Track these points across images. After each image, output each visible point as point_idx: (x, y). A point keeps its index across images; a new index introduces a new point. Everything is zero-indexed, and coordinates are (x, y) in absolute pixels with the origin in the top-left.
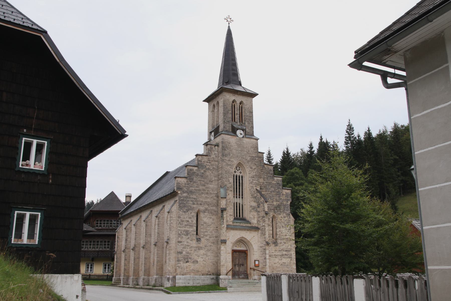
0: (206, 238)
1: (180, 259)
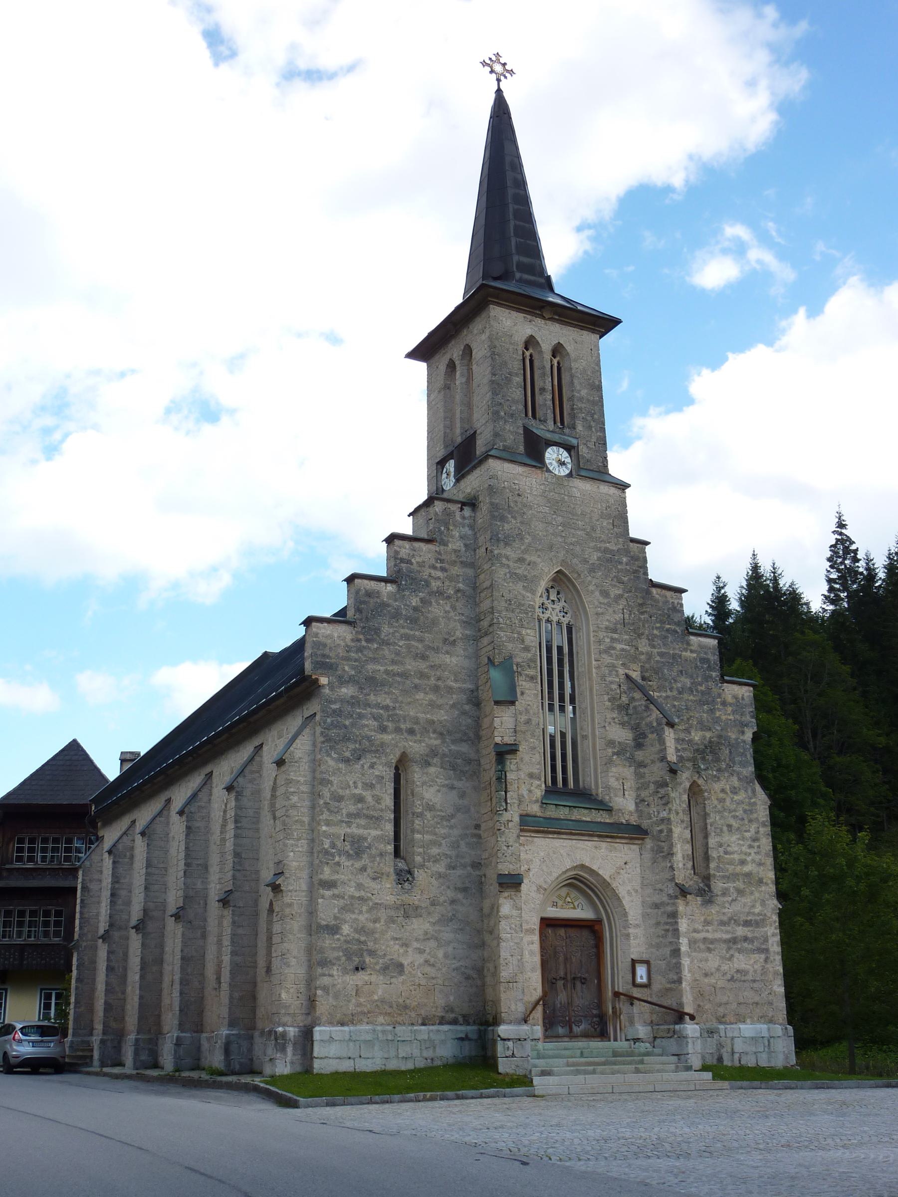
0: (435, 869)
1: (332, 955)
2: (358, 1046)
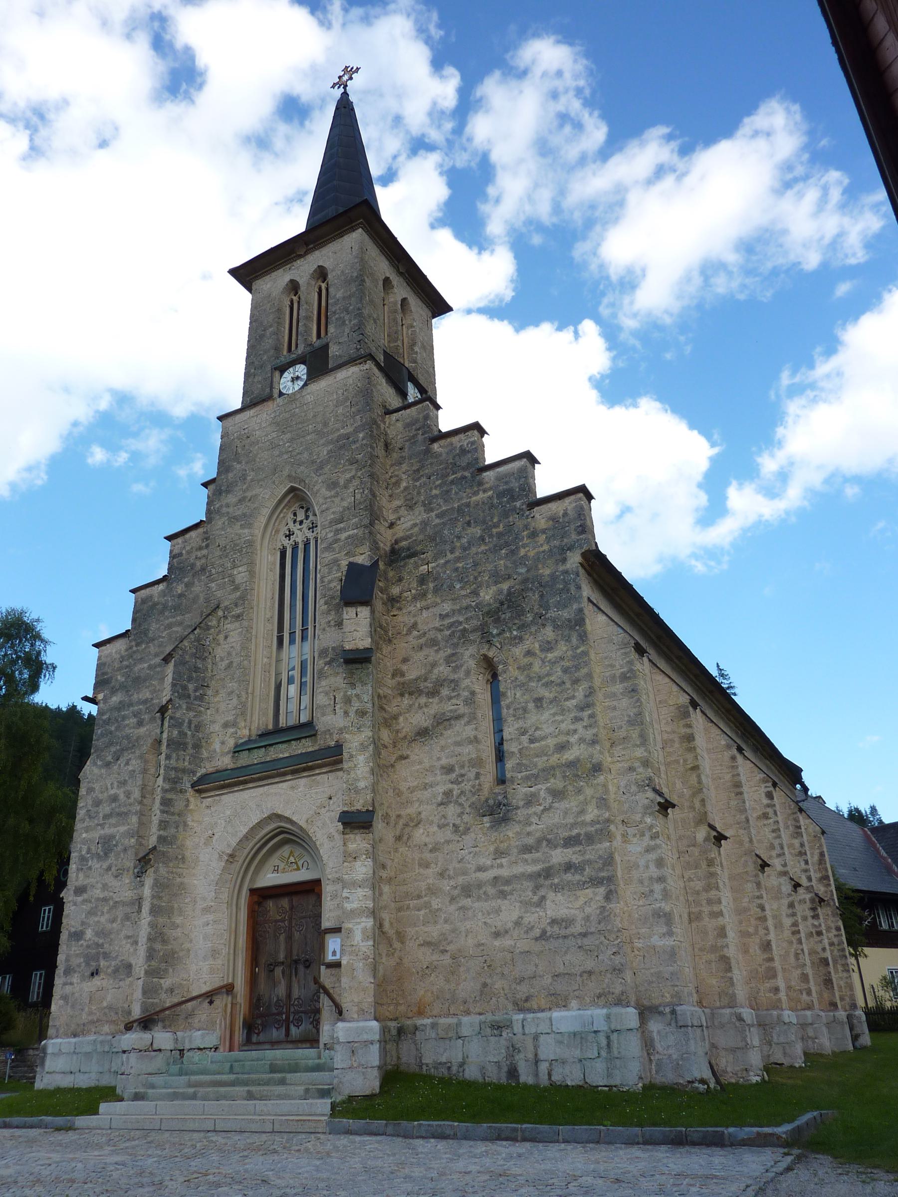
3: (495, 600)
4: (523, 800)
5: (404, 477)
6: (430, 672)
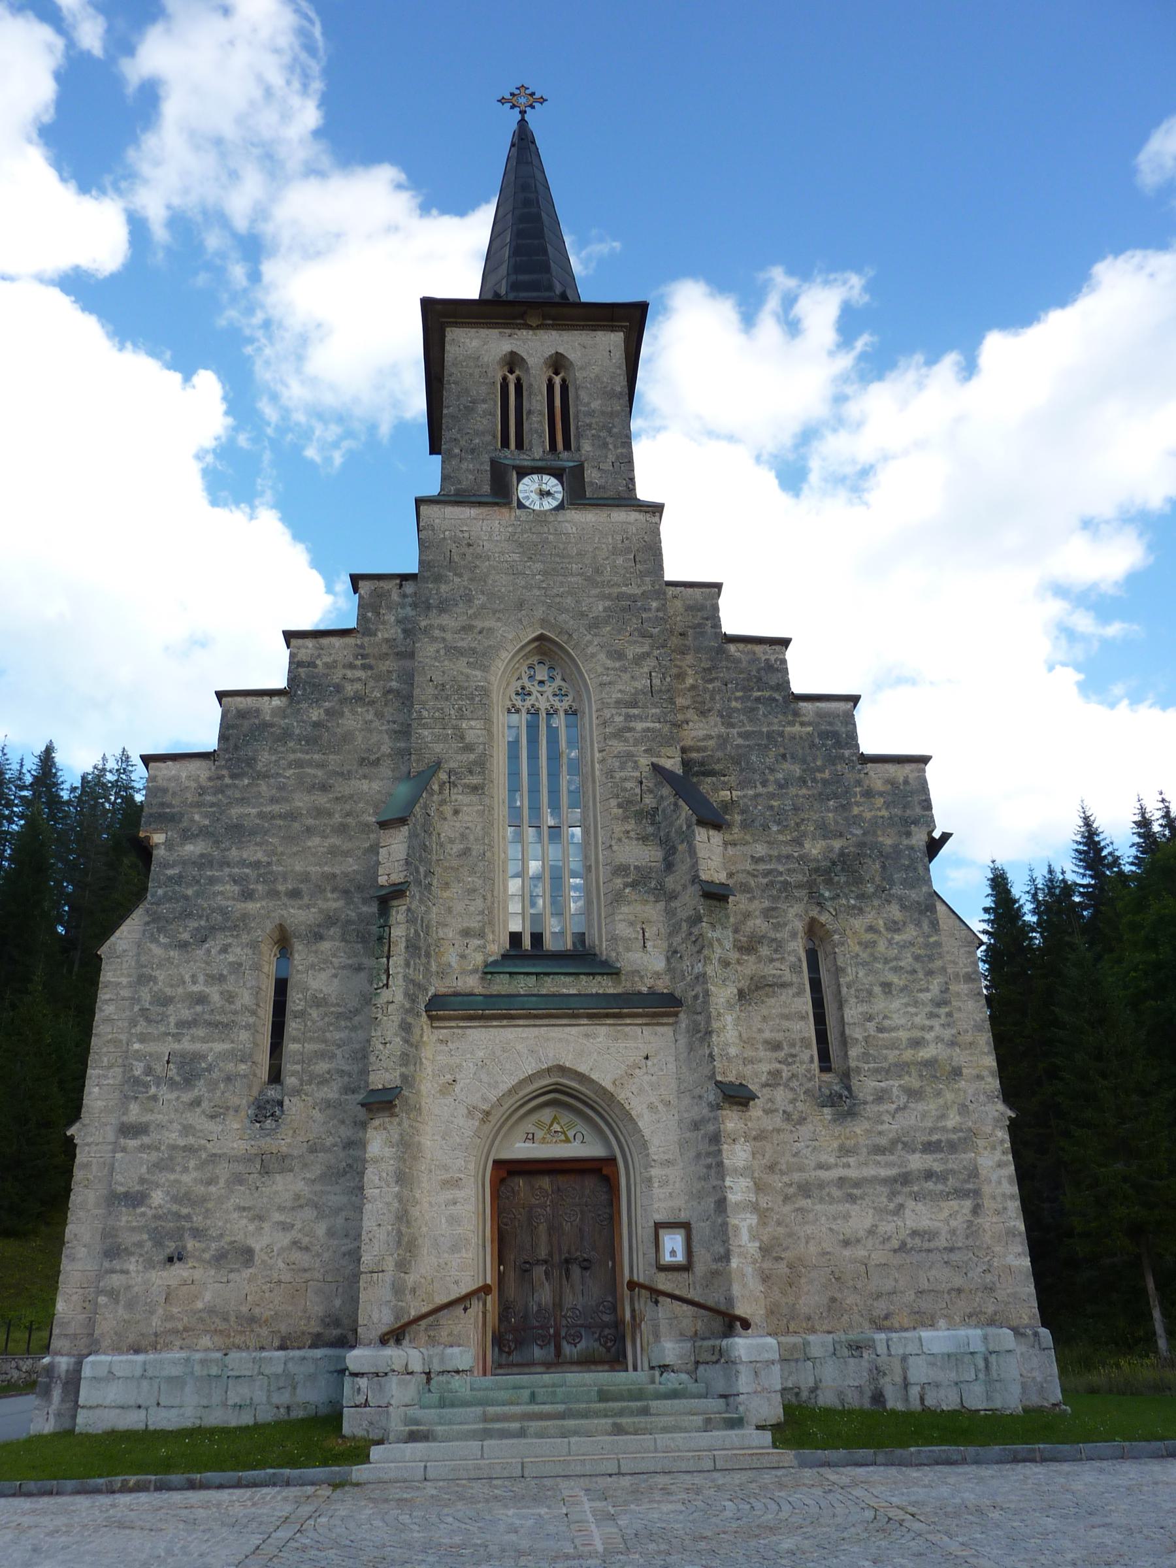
1: (128, 1239)
2: (156, 1386)
3: (826, 858)
4: (872, 1095)
5: (690, 672)
6: (743, 922)
